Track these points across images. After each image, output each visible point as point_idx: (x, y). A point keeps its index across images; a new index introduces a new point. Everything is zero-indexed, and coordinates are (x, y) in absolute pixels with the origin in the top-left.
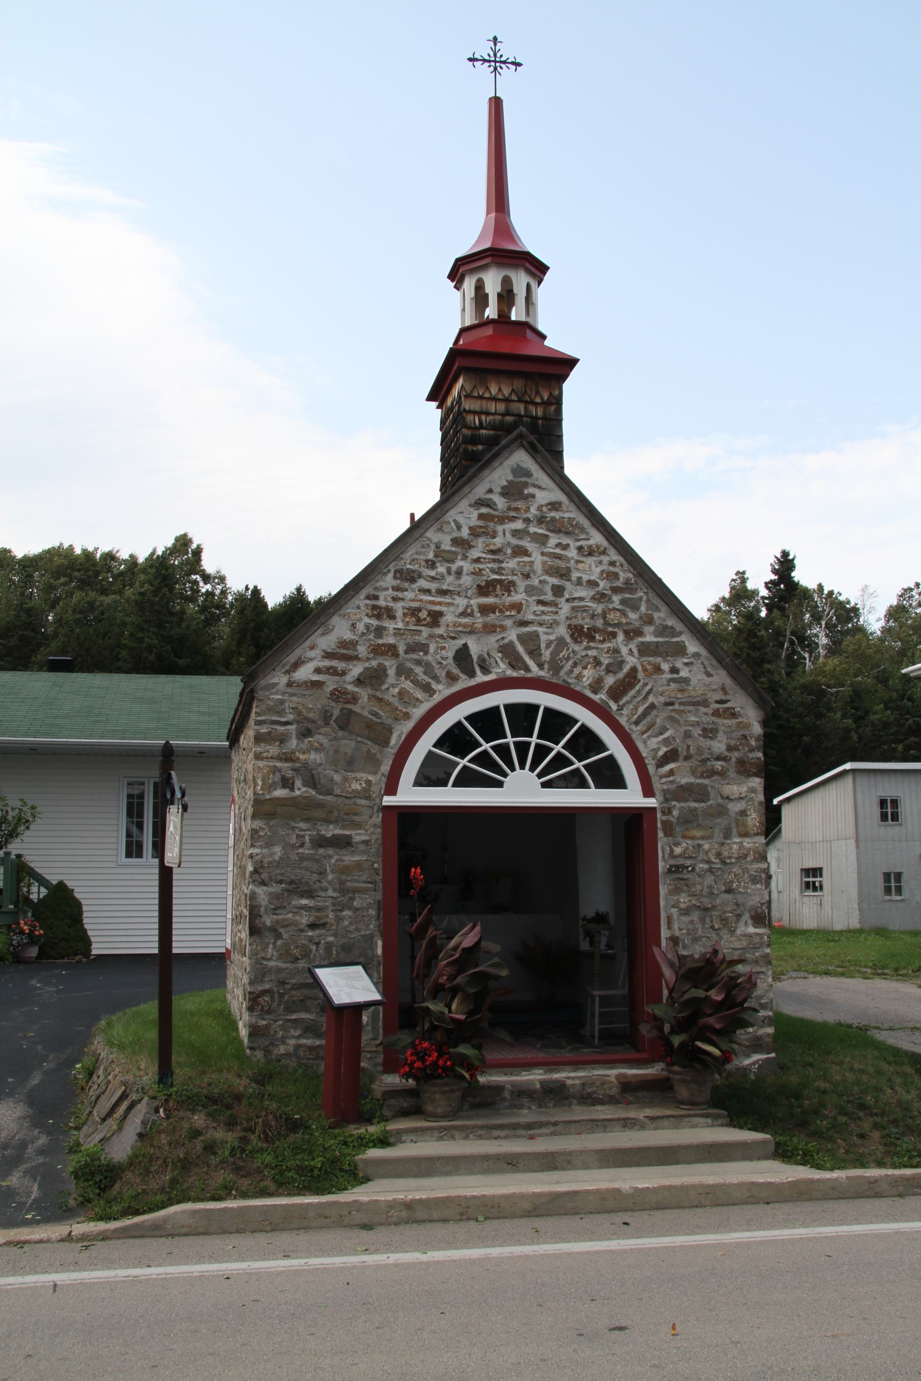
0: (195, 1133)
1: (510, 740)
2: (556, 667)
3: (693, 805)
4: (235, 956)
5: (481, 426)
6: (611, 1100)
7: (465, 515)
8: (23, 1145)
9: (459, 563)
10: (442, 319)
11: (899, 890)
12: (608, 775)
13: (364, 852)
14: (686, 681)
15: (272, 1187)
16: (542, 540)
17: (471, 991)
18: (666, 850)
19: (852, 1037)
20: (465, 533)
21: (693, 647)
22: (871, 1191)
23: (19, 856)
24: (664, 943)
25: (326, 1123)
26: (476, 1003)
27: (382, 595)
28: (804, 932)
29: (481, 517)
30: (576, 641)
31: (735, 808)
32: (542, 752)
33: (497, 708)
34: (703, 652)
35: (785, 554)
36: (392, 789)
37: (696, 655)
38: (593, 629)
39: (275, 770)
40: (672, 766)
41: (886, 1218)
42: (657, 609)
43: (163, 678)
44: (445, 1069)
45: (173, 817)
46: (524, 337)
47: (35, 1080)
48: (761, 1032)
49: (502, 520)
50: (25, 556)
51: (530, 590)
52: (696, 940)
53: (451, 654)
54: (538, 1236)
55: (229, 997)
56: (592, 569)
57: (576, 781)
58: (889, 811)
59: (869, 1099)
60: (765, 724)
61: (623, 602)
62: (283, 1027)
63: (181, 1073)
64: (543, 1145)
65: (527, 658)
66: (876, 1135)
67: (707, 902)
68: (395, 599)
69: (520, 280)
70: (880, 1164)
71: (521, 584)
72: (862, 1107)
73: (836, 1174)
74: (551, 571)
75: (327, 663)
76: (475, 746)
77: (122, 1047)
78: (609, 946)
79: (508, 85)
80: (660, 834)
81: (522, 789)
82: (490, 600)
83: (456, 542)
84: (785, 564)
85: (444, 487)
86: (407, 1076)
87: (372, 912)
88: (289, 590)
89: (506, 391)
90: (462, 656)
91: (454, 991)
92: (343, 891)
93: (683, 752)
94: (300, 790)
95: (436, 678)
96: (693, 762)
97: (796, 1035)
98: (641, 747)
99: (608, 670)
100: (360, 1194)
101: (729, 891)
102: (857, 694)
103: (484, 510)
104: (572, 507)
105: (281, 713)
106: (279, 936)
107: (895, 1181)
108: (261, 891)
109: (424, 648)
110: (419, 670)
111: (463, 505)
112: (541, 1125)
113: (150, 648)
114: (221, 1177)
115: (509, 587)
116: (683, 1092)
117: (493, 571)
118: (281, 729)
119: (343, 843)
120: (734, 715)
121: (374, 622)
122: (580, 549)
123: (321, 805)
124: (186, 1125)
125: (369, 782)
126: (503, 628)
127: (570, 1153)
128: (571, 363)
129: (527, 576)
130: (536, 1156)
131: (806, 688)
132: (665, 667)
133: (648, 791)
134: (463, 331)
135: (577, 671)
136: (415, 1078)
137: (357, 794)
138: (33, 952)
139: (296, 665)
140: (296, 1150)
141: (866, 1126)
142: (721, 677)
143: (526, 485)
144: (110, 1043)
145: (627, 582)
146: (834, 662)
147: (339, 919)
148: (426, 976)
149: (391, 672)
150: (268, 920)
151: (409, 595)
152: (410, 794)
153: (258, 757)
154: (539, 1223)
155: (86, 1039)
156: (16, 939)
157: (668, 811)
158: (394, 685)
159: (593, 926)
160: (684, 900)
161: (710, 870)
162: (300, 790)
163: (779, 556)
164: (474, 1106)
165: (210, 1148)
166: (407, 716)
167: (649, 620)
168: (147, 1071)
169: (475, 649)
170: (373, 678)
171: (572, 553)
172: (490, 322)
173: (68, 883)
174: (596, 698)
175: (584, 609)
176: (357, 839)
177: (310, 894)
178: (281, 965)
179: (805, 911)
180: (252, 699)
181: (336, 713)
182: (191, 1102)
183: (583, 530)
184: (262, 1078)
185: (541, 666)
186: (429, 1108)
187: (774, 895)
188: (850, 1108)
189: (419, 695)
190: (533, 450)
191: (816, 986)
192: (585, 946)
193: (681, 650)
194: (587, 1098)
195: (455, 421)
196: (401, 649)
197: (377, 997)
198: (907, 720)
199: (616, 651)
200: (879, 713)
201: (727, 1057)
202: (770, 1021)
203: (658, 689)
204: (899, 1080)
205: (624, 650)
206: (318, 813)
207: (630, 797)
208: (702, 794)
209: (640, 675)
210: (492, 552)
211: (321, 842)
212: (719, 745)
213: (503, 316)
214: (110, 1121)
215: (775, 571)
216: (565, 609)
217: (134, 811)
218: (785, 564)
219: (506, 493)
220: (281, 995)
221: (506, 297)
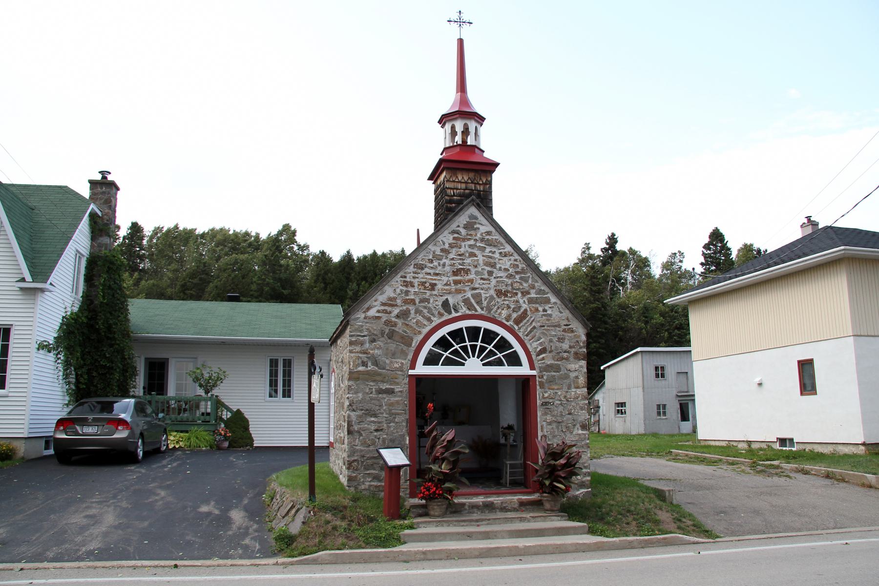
0: (328, 522)
1: (468, 343)
2: (489, 310)
3: (553, 374)
4: (337, 445)
5: (454, 195)
6: (515, 510)
7: (446, 238)
8: (247, 528)
9: (444, 260)
10: (434, 144)
11: (664, 413)
12: (514, 360)
13: (400, 396)
14: (550, 315)
15: (363, 545)
16: (483, 249)
17: (452, 459)
18: (540, 395)
19: (630, 483)
20: (447, 246)
21: (553, 299)
22: (630, 546)
23: (217, 396)
24: (539, 438)
25: (386, 519)
26: (454, 464)
27: (408, 276)
28: (615, 436)
29: (454, 238)
30: (498, 297)
31: (573, 375)
32: (482, 349)
33: (461, 329)
34: (559, 302)
36: (413, 367)
37: (555, 303)
38: (507, 291)
39: (359, 358)
40: (543, 355)
41: (634, 555)
42: (537, 282)
43: (286, 305)
44: (439, 495)
45: (315, 380)
46: (474, 152)
47: (246, 501)
48: (584, 479)
49: (464, 240)
51: (477, 273)
52: (554, 437)
53: (440, 304)
55: (331, 465)
56: (506, 263)
57: (499, 363)
58: (660, 372)
59: (632, 508)
60: (588, 335)
61: (521, 278)
62: (363, 477)
63: (319, 496)
64: (482, 529)
65: (475, 305)
66: (634, 523)
67: (560, 419)
68: (414, 278)
69: (472, 125)
70: (635, 535)
71: (473, 270)
72: (629, 511)
73: (614, 539)
74: (487, 264)
75: (383, 308)
76: (451, 346)
77: (287, 486)
78: (514, 441)
80: (538, 387)
81: (474, 367)
82: (458, 278)
83: (442, 250)
84: (612, 240)
85: (436, 227)
86: (422, 498)
87: (404, 424)
88: (344, 252)
89: (466, 178)
90: (446, 304)
91: (443, 460)
92: (391, 414)
93: (548, 349)
94: (371, 367)
95: (433, 314)
96: (554, 354)
97: (600, 481)
98: (529, 347)
99: (514, 311)
100: (403, 548)
101: (570, 414)
102: (646, 309)
103: (456, 235)
104: (497, 234)
105: (361, 331)
106: (361, 435)
107: (640, 542)
108: (353, 414)
109: (428, 301)
110: (425, 311)
111: (446, 233)
112: (482, 520)
113: (268, 284)
114: (341, 540)
115: (467, 271)
116: (547, 506)
117: (460, 264)
118: (362, 338)
119: (390, 392)
120: (572, 331)
121: (404, 289)
122: (501, 253)
123: (380, 374)
124: (323, 519)
125: (402, 363)
126: (465, 291)
127: (496, 532)
128: (496, 165)
129: (476, 267)
130: (480, 533)
132: (541, 309)
133: (532, 367)
134: (445, 149)
135: (499, 311)
136: (425, 499)
137: (397, 369)
138: (226, 444)
139: (368, 309)
140: (373, 529)
141: (630, 519)
142: (567, 313)
143: (475, 223)
144: (281, 485)
145: (523, 269)
146: (635, 293)
147: (389, 427)
148: (431, 453)
149: (412, 312)
150: (356, 428)
151: (420, 276)
152: (421, 369)
153: (351, 352)
154: (482, 560)
155: (265, 485)
156: (218, 438)
158: (414, 318)
159: (506, 431)
160: (549, 418)
161: (561, 404)
162: (371, 367)
164: (452, 513)
165: (335, 528)
166: (420, 333)
167: (533, 287)
168: (303, 496)
169: (451, 301)
171: (497, 255)
172: (458, 145)
173: (242, 411)
174: (508, 324)
175: (503, 282)
176: (397, 390)
177: (375, 416)
178: (363, 448)
179: (617, 425)
180: (347, 324)
181: (387, 331)
182: (325, 509)
183: (502, 244)
184: (355, 499)
185: (482, 309)
186: (432, 513)
187: (601, 417)
188: (623, 512)
189: (426, 323)
190: (478, 207)
191: (617, 461)
192: (502, 441)
193: (548, 301)
194: (504, 509)
195: (441, 192)
196: (417, 301)
197: (408, 463)
199: (518, 301)
200: (658, 319)
201: (568, 489)
202: (589, 474)
203: (537, 319)
204: (647, 500)
205: (521, 301)
206: (378, 378)
207: (524, 370)
208: (557, 369)
209: (529, 313)
210: (459, 255)
211: (380, 391)
212: (565, 346)
213: (464, 141)
214: (287, 518)
215: (607, 244)
216: (494, 282)
217: (273, 374)
218: (612, 240)
219: (466, 227)
220: (362, 462)
221: (466, 132)
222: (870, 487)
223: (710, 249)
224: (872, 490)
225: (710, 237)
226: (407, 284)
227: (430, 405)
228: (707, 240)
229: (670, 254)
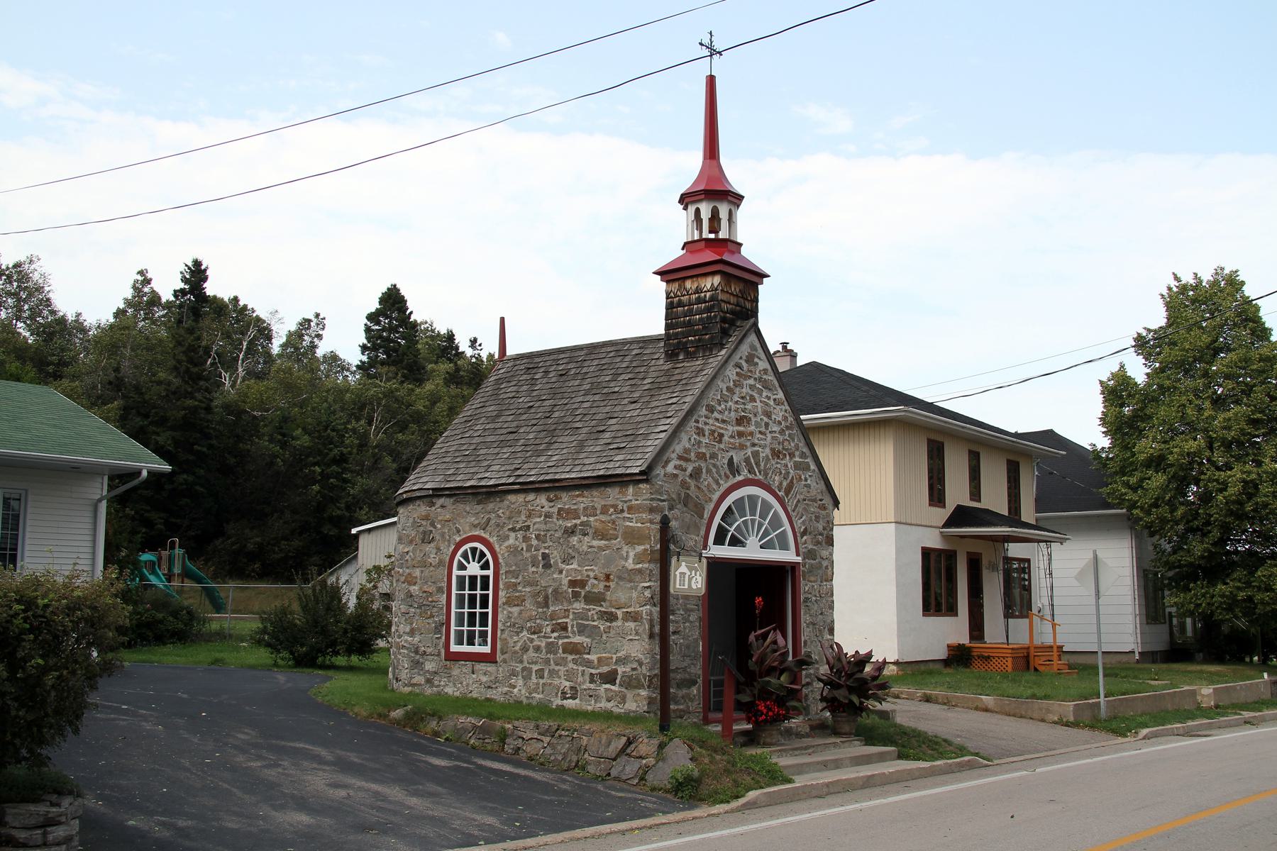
6: (807, 735)
35: (197, 263)
50: (215, 297)
54: (743, 822)
79: (719, 67)
82: (741, 429)
84: (197, 274)
105: (661, 494)
131: (227, 407)
157: (804, 566)
158: (706, 480)
163: (190, 264)
170: (696, 474)
171: (771, 403)
193: (808, 468)
198: (331, 450)
215: (184, 280)
218: (197, 274)
221: (715, 217)
222: (986, 710)
223: (378, 323)
224: (988, 714)
225: (382, 301)
226: (700, 432)
227: (758, 600)
228: (374, 305)
229: (299, 319)
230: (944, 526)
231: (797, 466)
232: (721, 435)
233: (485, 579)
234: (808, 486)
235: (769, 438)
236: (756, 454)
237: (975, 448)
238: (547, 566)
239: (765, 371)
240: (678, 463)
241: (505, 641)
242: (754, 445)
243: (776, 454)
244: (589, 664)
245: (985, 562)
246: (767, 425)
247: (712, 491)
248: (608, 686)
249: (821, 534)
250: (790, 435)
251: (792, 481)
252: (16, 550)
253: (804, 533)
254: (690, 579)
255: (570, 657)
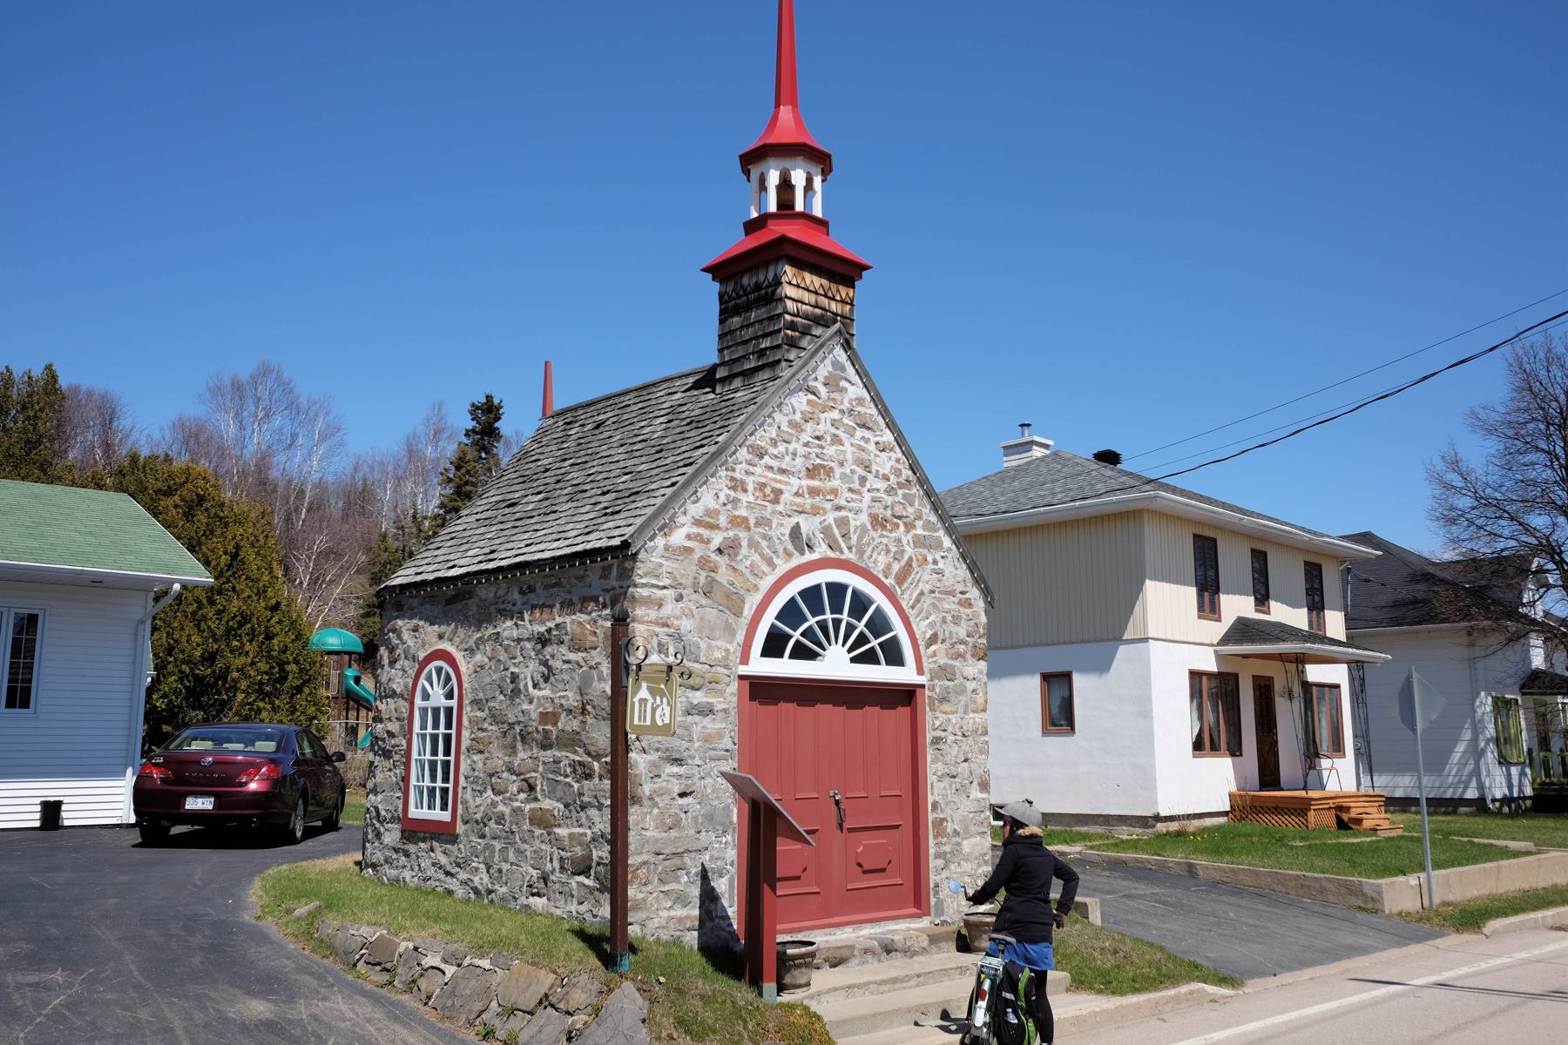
82: (815, 483)
157: (932, 689)
171: (872, 447)
193: (939, 546)
230: (1218, 644)
231: (918, 542)
232: (778, 493)
233: (449, 711)
234: (939, 572)
235: (867, 497)
236: (842, 523)
237: (1259, 546)
238: (516, 692)
239: (860, 401)
240: (695, 530)
241: (465, 802)
242: (839, 508)
243: (878, 522)
244: (556, 842)
245: (1278, 686)
246: (863, 480)
247: (760, 575)
248: (581, 879)
249: (962, 642)
250: (905, 496)
251: (909, 563)
252: (30, 681)
253: (933, 640)
254: (654, 711)
255: (538, 832)
